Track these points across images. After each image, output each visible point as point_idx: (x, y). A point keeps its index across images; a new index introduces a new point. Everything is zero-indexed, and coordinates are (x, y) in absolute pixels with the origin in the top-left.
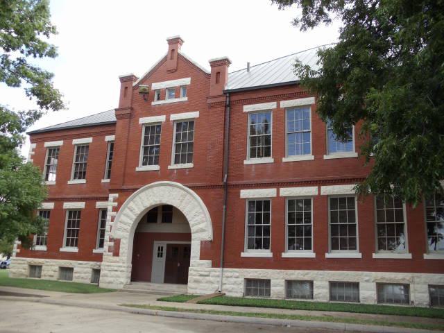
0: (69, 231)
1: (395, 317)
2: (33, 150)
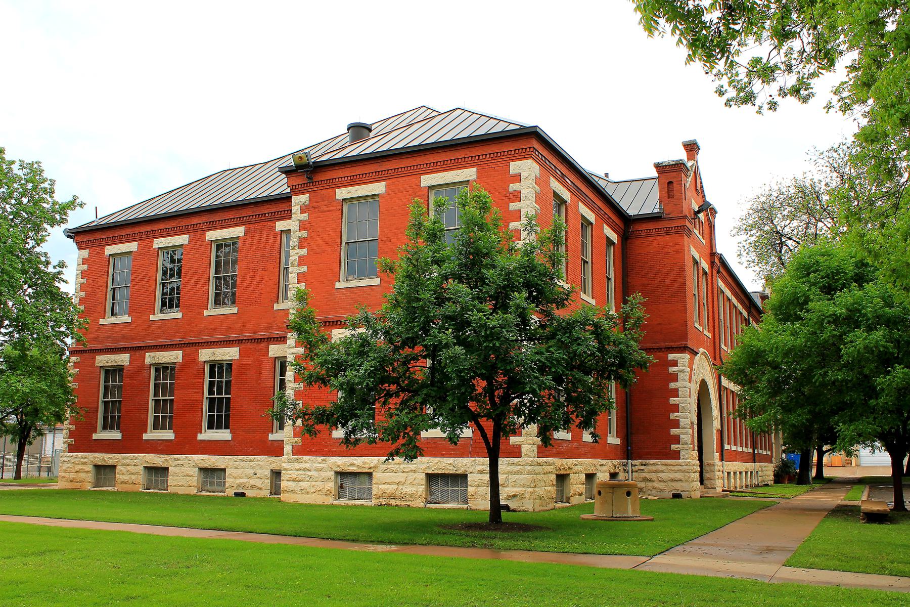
0: (212, 401)
1: (486, 491)
2: (84, 261)
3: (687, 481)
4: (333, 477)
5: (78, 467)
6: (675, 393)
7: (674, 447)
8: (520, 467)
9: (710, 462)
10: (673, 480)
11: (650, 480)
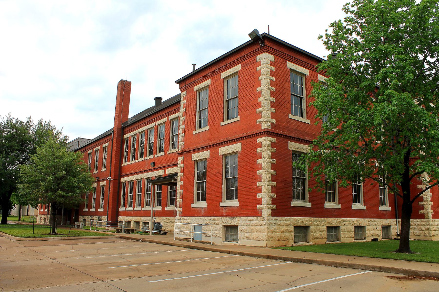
4: (222, 229)
5: (283, 229)
7: (421, 212)
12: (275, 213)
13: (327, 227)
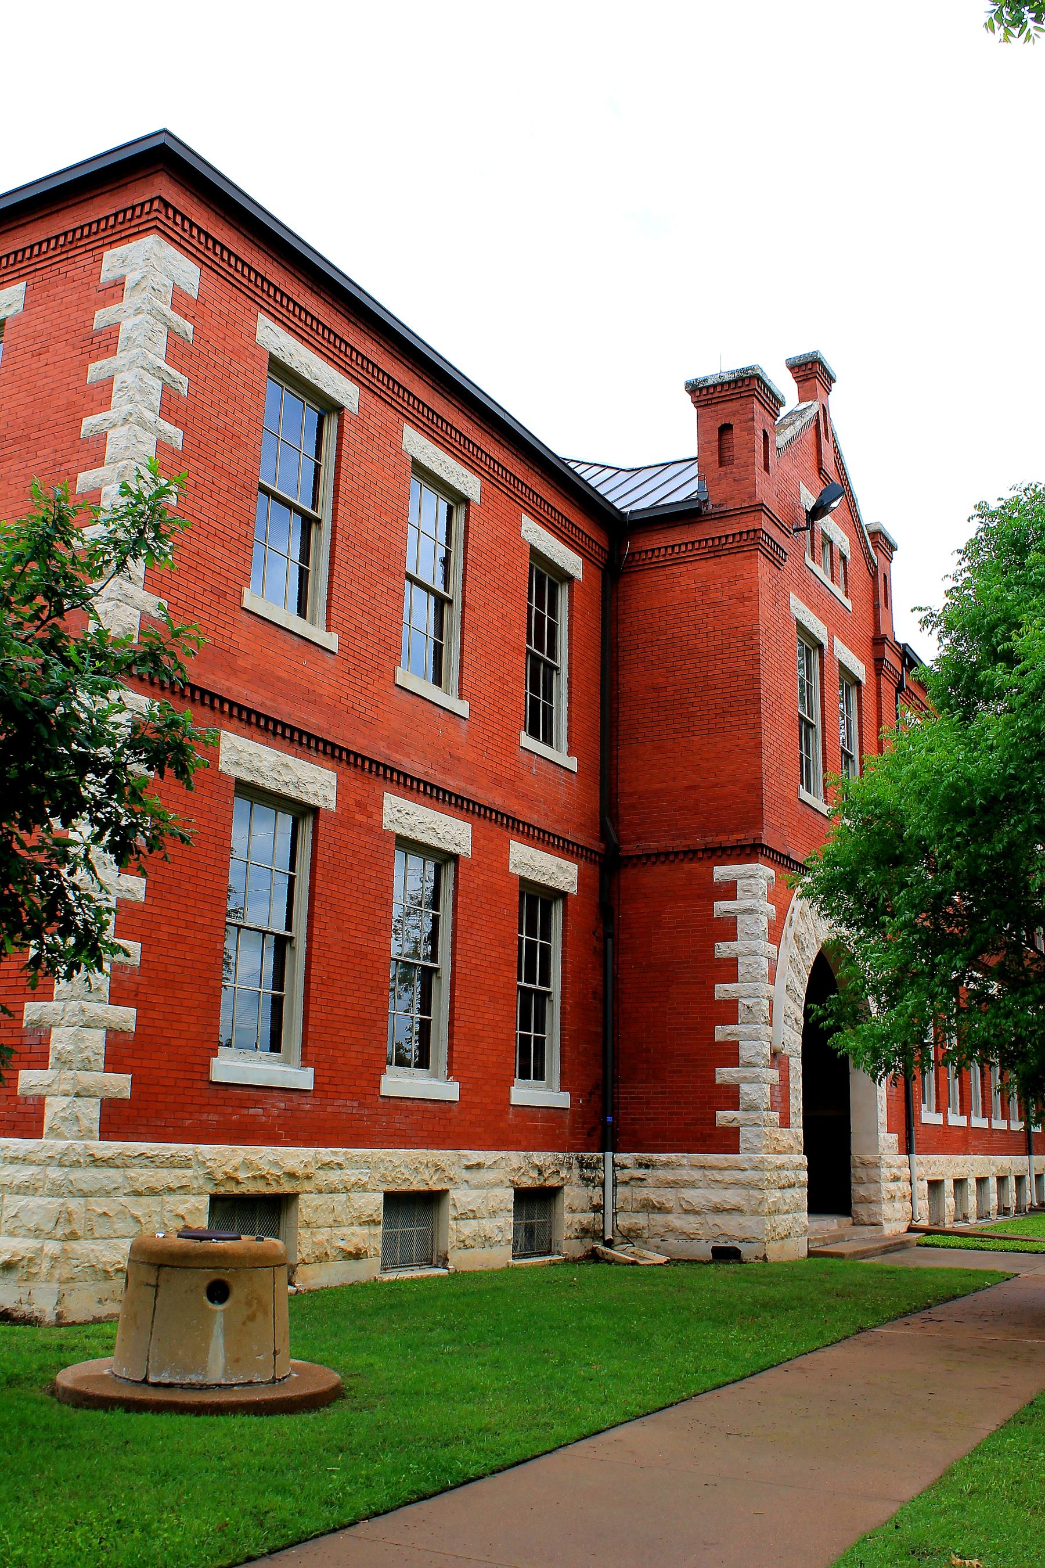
3: (755, 1213)
6: (729, 970)
7: (724, 1117)
8: (33, 1169)
9: (869, 1157)
10: (718, 1210)
11: (661, 1209)
12: (117, 1121)
13: (929, 1182)
